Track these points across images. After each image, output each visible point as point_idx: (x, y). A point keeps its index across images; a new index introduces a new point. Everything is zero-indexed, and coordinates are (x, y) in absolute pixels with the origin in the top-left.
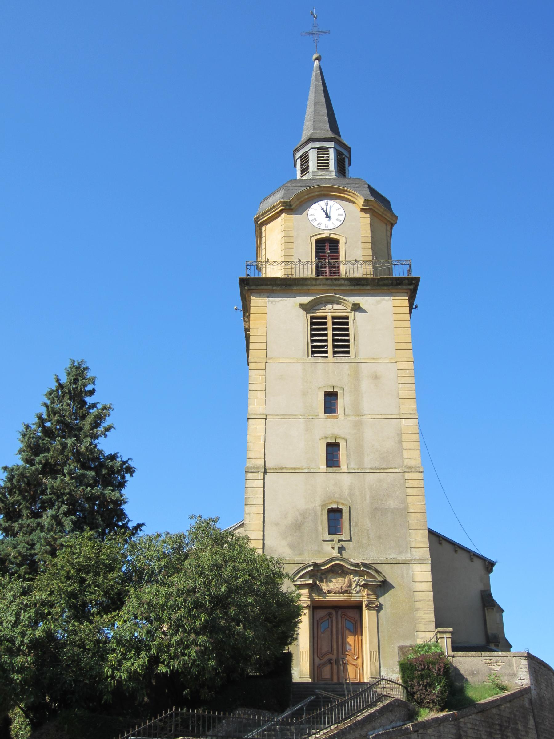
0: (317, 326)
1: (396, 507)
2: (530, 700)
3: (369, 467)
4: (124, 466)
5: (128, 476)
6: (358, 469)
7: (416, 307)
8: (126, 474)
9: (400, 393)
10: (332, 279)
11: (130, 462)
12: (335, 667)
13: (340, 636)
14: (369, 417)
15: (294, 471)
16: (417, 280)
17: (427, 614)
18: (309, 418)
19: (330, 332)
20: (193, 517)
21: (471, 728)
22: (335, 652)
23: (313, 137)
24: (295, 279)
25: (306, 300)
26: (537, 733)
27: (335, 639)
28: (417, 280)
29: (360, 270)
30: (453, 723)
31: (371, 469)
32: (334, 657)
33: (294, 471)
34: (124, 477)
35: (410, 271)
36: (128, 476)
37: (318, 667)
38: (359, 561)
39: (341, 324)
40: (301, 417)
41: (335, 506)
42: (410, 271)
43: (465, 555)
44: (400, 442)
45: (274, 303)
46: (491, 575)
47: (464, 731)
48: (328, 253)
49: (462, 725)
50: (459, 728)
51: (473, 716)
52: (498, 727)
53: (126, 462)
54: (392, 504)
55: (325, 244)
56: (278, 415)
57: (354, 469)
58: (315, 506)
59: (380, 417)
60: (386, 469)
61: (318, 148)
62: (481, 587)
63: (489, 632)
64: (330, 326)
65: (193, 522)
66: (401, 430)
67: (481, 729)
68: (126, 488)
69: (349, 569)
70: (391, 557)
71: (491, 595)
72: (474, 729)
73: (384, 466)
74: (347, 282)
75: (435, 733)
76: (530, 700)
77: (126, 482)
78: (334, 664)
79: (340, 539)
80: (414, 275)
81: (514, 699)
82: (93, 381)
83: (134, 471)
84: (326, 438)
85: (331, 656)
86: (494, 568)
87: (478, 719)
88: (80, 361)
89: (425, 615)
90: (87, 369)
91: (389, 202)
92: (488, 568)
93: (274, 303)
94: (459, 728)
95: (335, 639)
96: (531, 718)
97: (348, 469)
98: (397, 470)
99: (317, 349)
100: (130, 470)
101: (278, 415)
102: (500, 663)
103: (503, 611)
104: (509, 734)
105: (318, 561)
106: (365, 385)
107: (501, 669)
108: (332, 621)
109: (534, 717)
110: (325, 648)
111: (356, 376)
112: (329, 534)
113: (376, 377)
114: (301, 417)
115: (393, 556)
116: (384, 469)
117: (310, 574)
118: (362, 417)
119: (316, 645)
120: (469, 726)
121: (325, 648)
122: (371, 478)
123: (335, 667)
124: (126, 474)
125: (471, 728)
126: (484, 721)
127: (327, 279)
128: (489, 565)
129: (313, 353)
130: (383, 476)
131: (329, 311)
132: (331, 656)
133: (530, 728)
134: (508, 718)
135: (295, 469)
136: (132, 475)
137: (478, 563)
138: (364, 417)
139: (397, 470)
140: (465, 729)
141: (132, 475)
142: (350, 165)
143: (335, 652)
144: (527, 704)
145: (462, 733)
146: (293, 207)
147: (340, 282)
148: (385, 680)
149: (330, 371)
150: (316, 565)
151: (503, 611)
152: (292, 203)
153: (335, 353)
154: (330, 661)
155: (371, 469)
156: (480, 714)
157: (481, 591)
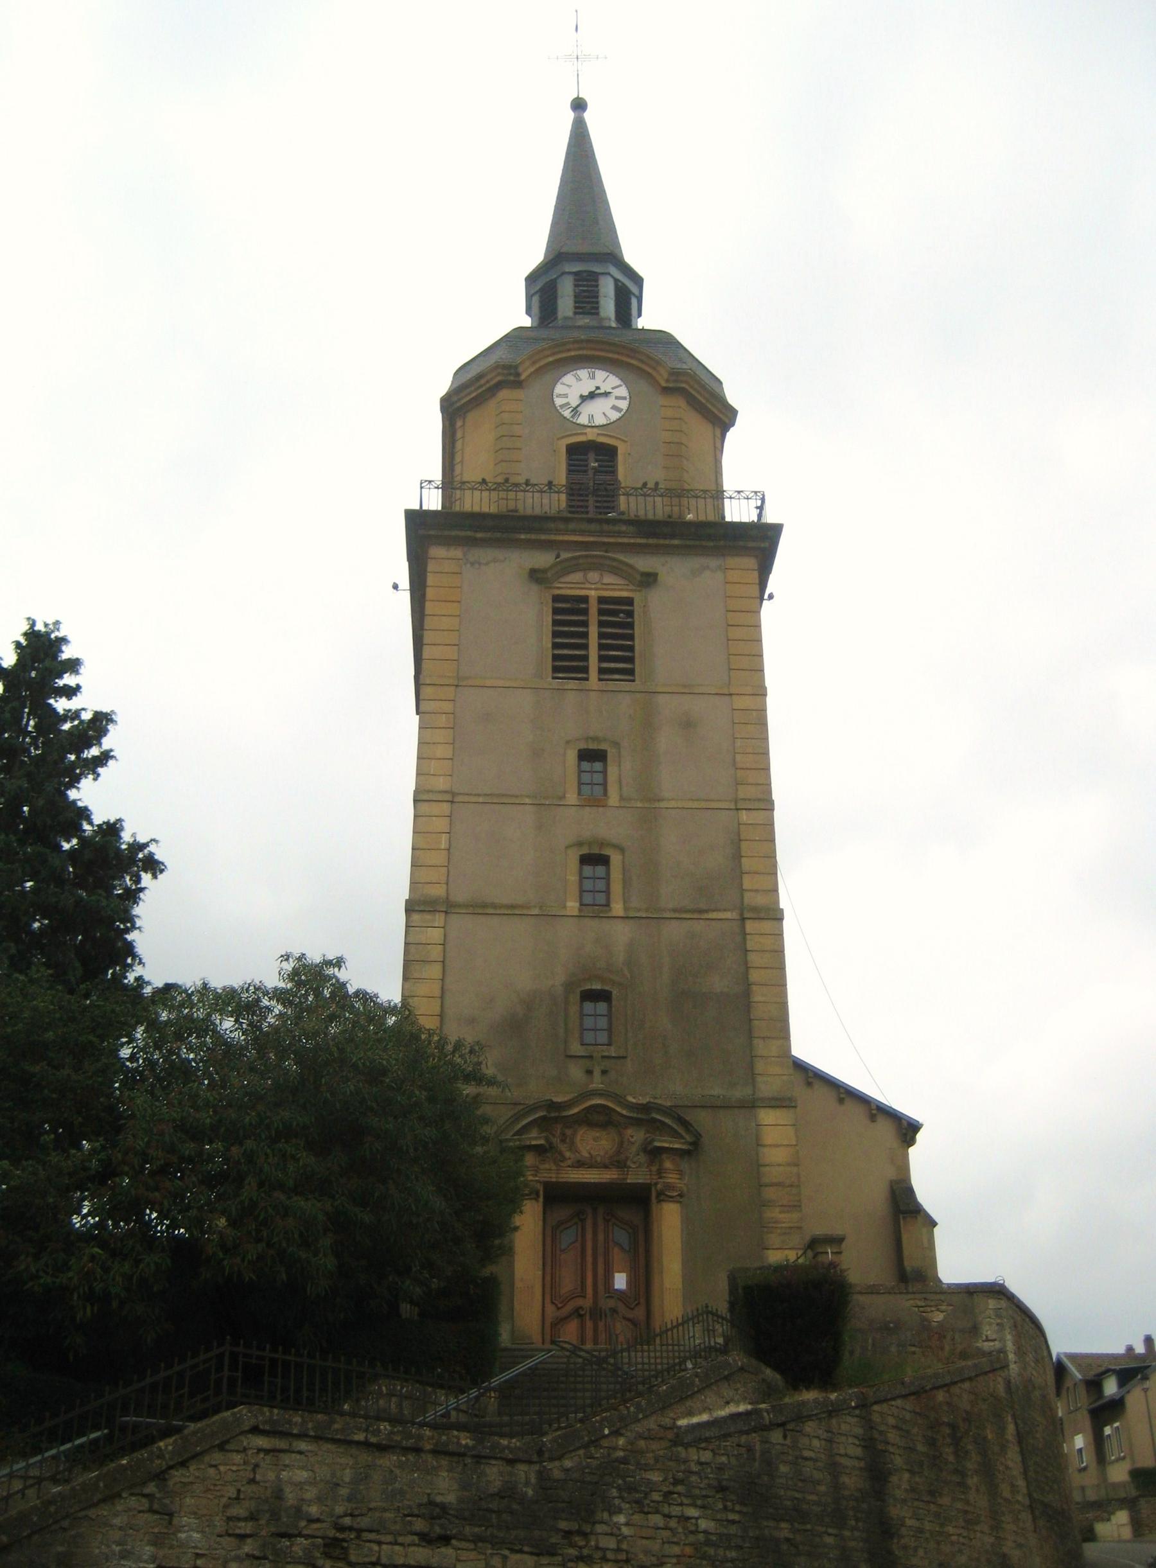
0: (568, 614)
1: (726, 990)
2: (1008, 1383)
3: (671, 906)
4: (140, 856)
5: (146, 878)
6: (647, 910)
7: (771, 597)
8: (143, 874)
9: (738, 757)
10: (600, 521)
11: (152, 848)
12: (589, 1324)
13: (601, 1260)
14: (673, 804)
15: (512, 910)
16: (777, 529)
17: (788, 1212)
18: (546, 802)
19: (593, 631)
20: (286, 957)
21: (894, 1427)
22: (589, 1291)
23: (564, 250)
24: (525, 518)
25: (543, 559)
26: (1022, 1453)
27: (589, 1266)
28: (777, 529)
29: (659, 505)
30: (857, 1412)
31: (675, 910)
32: (587, 1303)
33: (512, 910)
34: (138, 880)
35: (761, 508)
36: (146, 878)
37: (554, 1325)
38: (643, 1100)
39: (619, 619)
40: (527, 801)
41: (597, 986)
42: (761, 508)
43: (859, 1111)
44: (738, 856)
45: (477, 566)
46: (911, 1150)
47: (881, 1433)
48: (594, 468)
49: (876, 1418)
50: (869, 1426)
51: (899, 1402)
52: (948, 1431)
53: (146, 845)
54: (718, 983)
55: (586, 454)
56: (479, 795)
57: (639, 910)
58: (553, 986)
59: (696, 805)
60: (707, 911)
61: (576, 274)
62: (891, 1173)
63: (906, 1263)
64: (593, 618)
65: (288, 966)
66: (739, 835)
67: (915, 1430)
68: (141, 903)
69: (623, 1116)
70: (713, 1092)
71: (911, 1191)
72: (901, 1429)
73: (702, 906)
74: (631, 529)
75: (820, 1432)
76: (1008, 1383)
77: (142, 890)
78: (588, 1317)
79: (606, 1054)
80: (770, 518)
81: (977, 1376)
82: (73, 665)
83: (162, 871)
84: (580, 844)
85: (580, 1302)
86: (919, 1136)
87: (908, 1408)
88: (50, 621)
89: (782, 1216)
90: (63, 640)
91: (721, 383)
92: (905, 1135)
93: (477, 566)
94: (869, 1426)
95: (589, 1266)
96: (1010, 1419)
97: (626, 909)
98: (728, 915)
99: (567, 663)
100: (153, 866)
101: (479, 795)
102: (944, 1308)
103: (934, 1224)
104: (969, 1447)
105: (558, 1099)
106: (666, 739)
107: (945, 1318)
108: (583, 1229)
109: (1014, 1417)
110: (568, 1284)
111: (648, 724)
112: (608, 857)
113: (688, 724)
114: (527, 801)
115: (717, 1091)
116: (701, 911)
117: (544, 1124)
118: (657, 805)
119: (548, 1278)
120: (891, 1421)
121: (568, 1284)
122: (674, 931)
123: (589, 1324)
124: (143, 874)
125: (894, 1427)
126: (919, 1414)
127: (590, 521)
128: (908, 1130)
129: (556, 669)
130: (698, 926)
131: (595, 586)
132: (580, 1302)
133: (1007, 1441)
134: (967, 1412)
135: (512, 907)
136: (155, 877)
137: (885, 1130)
138: (663, 804)
139: (728, 915)
140: (883, 1428)
141: (155, 877)
142: (640, 315)
143: (589, 1291)
144: (1001, 1389)
145: (876, 1436)
146: (523, 377)
147: (617, 528)
148: (713, 1314)
149: (594, 708)
150: (552, 1106)
151: (934, 1224)
152: (520, 370)
153: (601, 671)
154: (578, 1313)
155: (675, 910)
156: (912, 1397)
157: (891, 1182)
